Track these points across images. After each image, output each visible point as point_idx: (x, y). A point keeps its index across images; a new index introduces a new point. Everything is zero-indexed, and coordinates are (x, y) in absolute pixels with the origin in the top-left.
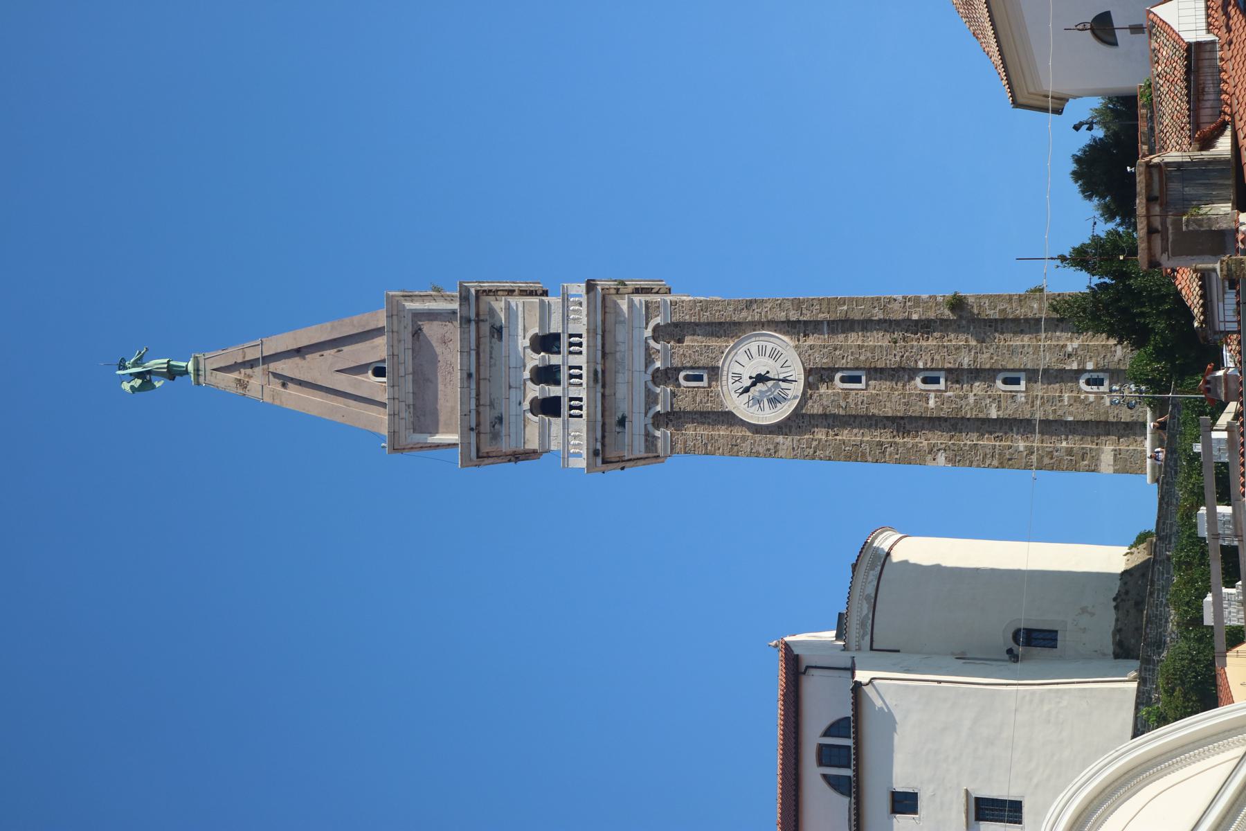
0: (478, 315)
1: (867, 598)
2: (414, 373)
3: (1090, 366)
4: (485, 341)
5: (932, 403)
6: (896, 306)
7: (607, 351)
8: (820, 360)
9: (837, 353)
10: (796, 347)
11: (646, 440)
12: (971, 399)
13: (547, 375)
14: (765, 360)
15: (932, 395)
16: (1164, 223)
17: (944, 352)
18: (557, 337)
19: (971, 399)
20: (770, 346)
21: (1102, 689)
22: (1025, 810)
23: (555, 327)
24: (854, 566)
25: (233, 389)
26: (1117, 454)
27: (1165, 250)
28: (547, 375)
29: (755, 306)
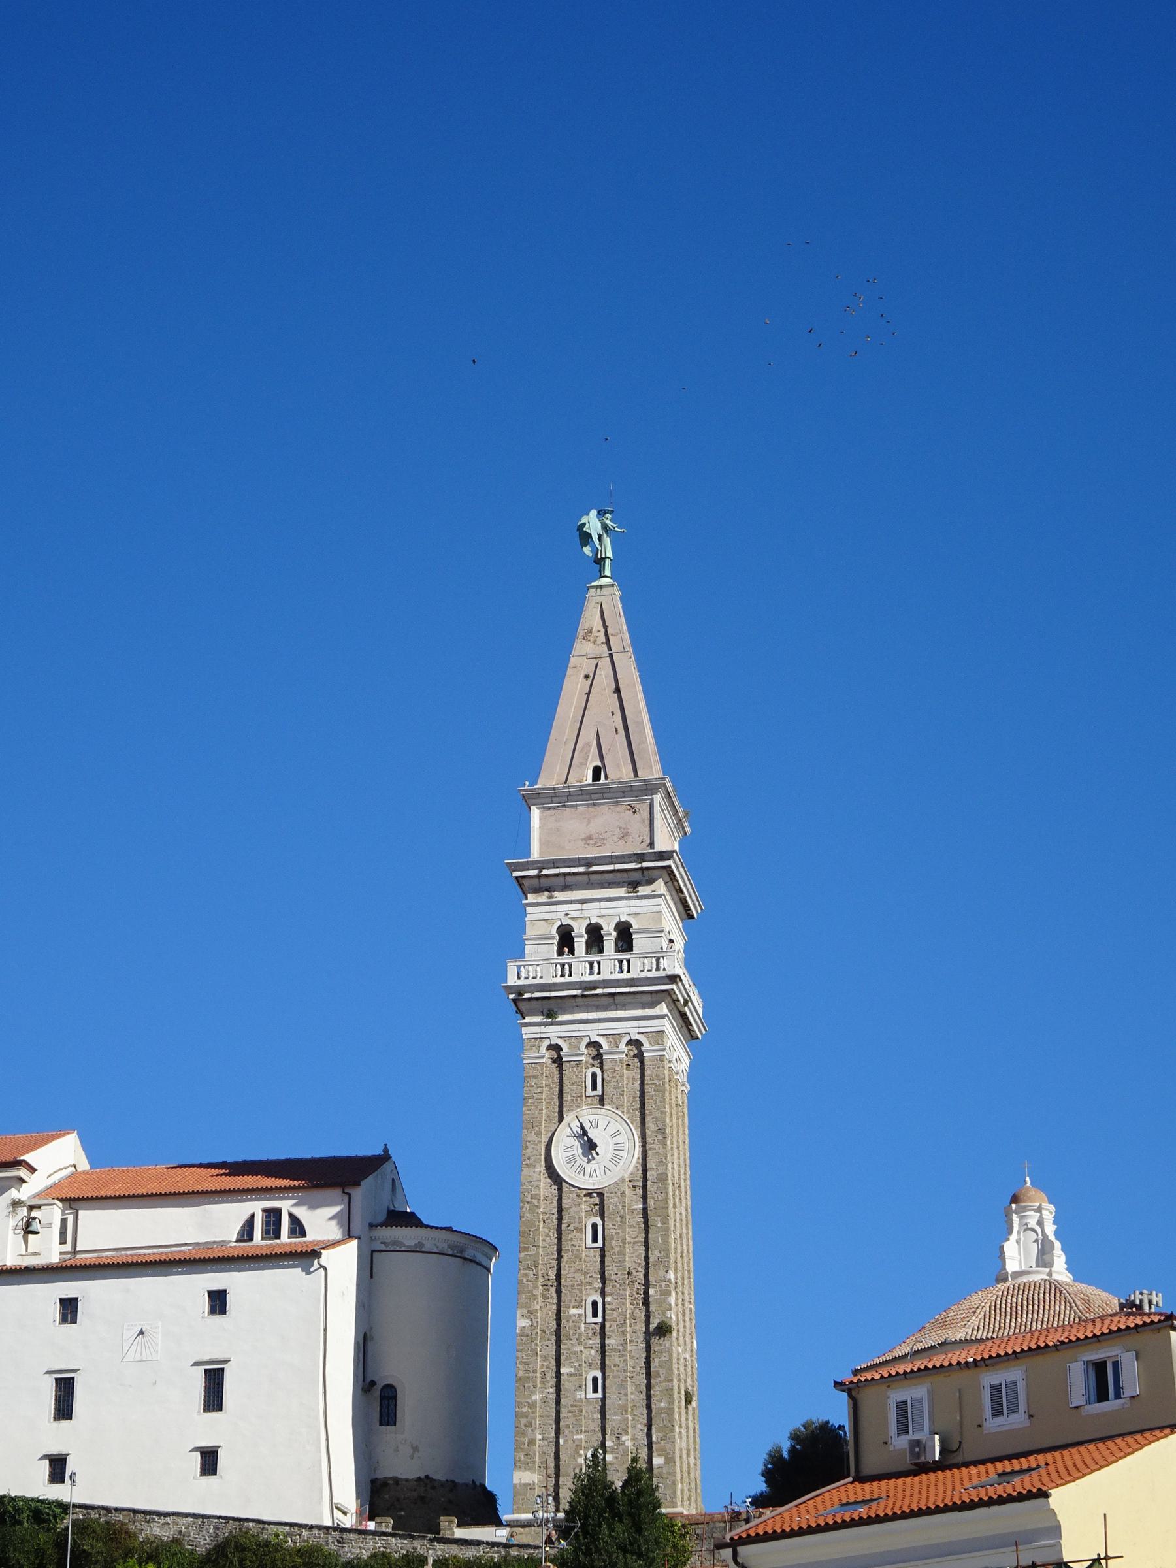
1: (420, 1244)
3: (609, 1458)
5: (573, 1311)
6: (661, 1273)
8: (611, 1202)
9: (618, 1219)
10: (623, 1180)
12: (577, 1349)
13: (595, 936)
14: (611, 1151)
17: (620, 1320)
19: (577, 1349)
20: (624, 1154)
21: (321, 1481)
22: (215, 1414)
23: (637, 942)
24: (449, 1229)
25: (583, 625)
26: (531, 1486)
28: (595, 936)
29: (660, 1137)
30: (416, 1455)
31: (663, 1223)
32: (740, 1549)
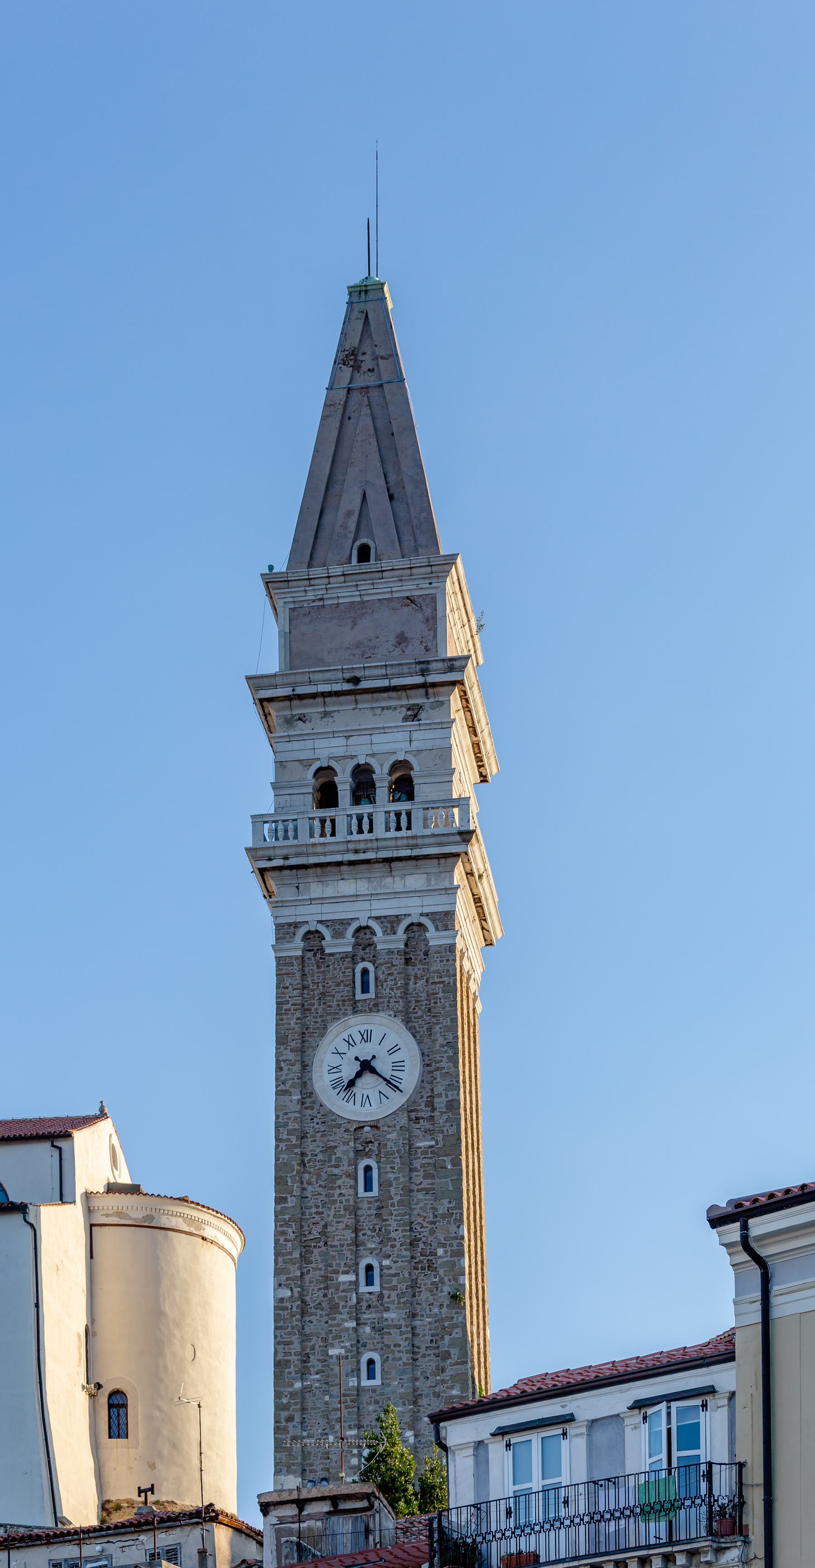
0: (434, 685)
2: (363, 602)
4: (402, 701)
7: (393, 865)
11: (290, 924)
15: (352, 1277)
16: (310, 1517)
18: (411, 797)
27: (282, 1520)
28: (363, 785)
30: (383, 1066)
31: (453, 1165)
32: (751, 1222)
